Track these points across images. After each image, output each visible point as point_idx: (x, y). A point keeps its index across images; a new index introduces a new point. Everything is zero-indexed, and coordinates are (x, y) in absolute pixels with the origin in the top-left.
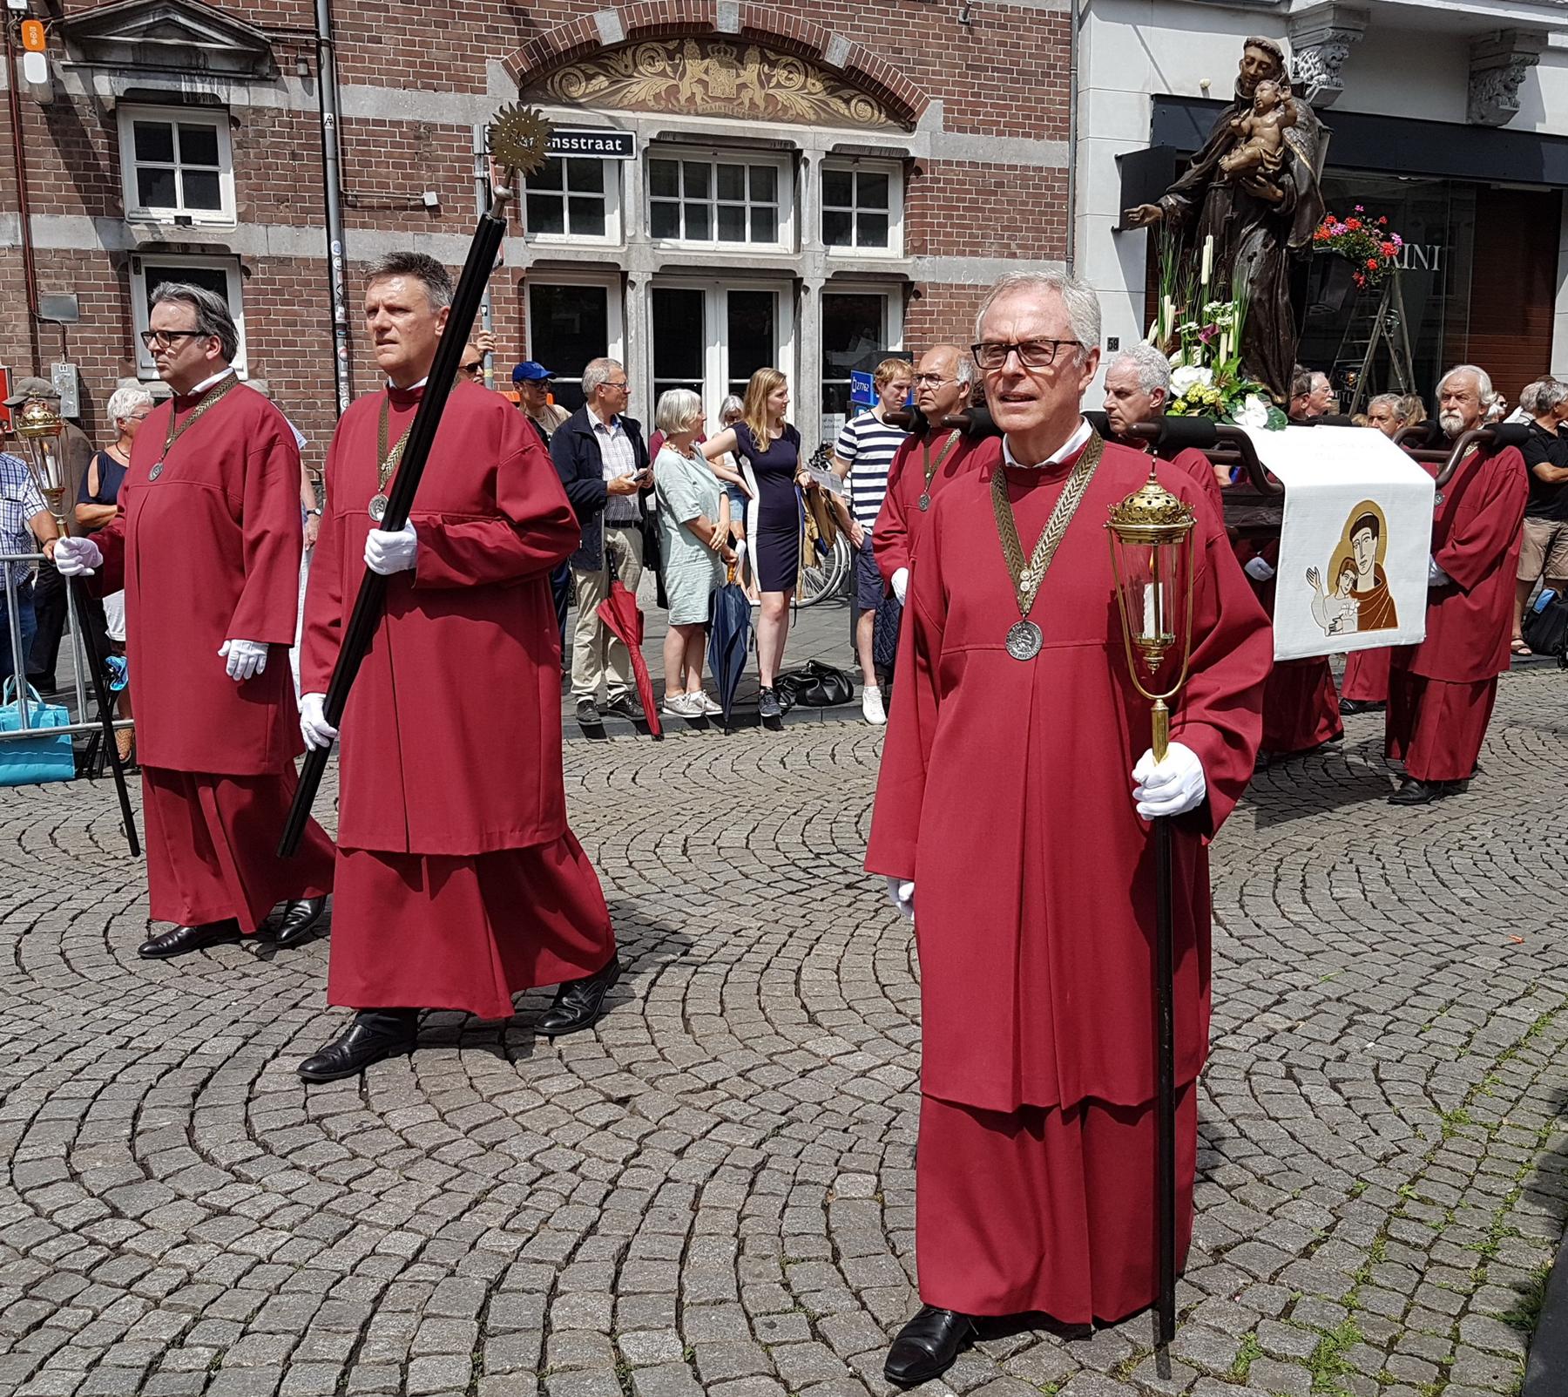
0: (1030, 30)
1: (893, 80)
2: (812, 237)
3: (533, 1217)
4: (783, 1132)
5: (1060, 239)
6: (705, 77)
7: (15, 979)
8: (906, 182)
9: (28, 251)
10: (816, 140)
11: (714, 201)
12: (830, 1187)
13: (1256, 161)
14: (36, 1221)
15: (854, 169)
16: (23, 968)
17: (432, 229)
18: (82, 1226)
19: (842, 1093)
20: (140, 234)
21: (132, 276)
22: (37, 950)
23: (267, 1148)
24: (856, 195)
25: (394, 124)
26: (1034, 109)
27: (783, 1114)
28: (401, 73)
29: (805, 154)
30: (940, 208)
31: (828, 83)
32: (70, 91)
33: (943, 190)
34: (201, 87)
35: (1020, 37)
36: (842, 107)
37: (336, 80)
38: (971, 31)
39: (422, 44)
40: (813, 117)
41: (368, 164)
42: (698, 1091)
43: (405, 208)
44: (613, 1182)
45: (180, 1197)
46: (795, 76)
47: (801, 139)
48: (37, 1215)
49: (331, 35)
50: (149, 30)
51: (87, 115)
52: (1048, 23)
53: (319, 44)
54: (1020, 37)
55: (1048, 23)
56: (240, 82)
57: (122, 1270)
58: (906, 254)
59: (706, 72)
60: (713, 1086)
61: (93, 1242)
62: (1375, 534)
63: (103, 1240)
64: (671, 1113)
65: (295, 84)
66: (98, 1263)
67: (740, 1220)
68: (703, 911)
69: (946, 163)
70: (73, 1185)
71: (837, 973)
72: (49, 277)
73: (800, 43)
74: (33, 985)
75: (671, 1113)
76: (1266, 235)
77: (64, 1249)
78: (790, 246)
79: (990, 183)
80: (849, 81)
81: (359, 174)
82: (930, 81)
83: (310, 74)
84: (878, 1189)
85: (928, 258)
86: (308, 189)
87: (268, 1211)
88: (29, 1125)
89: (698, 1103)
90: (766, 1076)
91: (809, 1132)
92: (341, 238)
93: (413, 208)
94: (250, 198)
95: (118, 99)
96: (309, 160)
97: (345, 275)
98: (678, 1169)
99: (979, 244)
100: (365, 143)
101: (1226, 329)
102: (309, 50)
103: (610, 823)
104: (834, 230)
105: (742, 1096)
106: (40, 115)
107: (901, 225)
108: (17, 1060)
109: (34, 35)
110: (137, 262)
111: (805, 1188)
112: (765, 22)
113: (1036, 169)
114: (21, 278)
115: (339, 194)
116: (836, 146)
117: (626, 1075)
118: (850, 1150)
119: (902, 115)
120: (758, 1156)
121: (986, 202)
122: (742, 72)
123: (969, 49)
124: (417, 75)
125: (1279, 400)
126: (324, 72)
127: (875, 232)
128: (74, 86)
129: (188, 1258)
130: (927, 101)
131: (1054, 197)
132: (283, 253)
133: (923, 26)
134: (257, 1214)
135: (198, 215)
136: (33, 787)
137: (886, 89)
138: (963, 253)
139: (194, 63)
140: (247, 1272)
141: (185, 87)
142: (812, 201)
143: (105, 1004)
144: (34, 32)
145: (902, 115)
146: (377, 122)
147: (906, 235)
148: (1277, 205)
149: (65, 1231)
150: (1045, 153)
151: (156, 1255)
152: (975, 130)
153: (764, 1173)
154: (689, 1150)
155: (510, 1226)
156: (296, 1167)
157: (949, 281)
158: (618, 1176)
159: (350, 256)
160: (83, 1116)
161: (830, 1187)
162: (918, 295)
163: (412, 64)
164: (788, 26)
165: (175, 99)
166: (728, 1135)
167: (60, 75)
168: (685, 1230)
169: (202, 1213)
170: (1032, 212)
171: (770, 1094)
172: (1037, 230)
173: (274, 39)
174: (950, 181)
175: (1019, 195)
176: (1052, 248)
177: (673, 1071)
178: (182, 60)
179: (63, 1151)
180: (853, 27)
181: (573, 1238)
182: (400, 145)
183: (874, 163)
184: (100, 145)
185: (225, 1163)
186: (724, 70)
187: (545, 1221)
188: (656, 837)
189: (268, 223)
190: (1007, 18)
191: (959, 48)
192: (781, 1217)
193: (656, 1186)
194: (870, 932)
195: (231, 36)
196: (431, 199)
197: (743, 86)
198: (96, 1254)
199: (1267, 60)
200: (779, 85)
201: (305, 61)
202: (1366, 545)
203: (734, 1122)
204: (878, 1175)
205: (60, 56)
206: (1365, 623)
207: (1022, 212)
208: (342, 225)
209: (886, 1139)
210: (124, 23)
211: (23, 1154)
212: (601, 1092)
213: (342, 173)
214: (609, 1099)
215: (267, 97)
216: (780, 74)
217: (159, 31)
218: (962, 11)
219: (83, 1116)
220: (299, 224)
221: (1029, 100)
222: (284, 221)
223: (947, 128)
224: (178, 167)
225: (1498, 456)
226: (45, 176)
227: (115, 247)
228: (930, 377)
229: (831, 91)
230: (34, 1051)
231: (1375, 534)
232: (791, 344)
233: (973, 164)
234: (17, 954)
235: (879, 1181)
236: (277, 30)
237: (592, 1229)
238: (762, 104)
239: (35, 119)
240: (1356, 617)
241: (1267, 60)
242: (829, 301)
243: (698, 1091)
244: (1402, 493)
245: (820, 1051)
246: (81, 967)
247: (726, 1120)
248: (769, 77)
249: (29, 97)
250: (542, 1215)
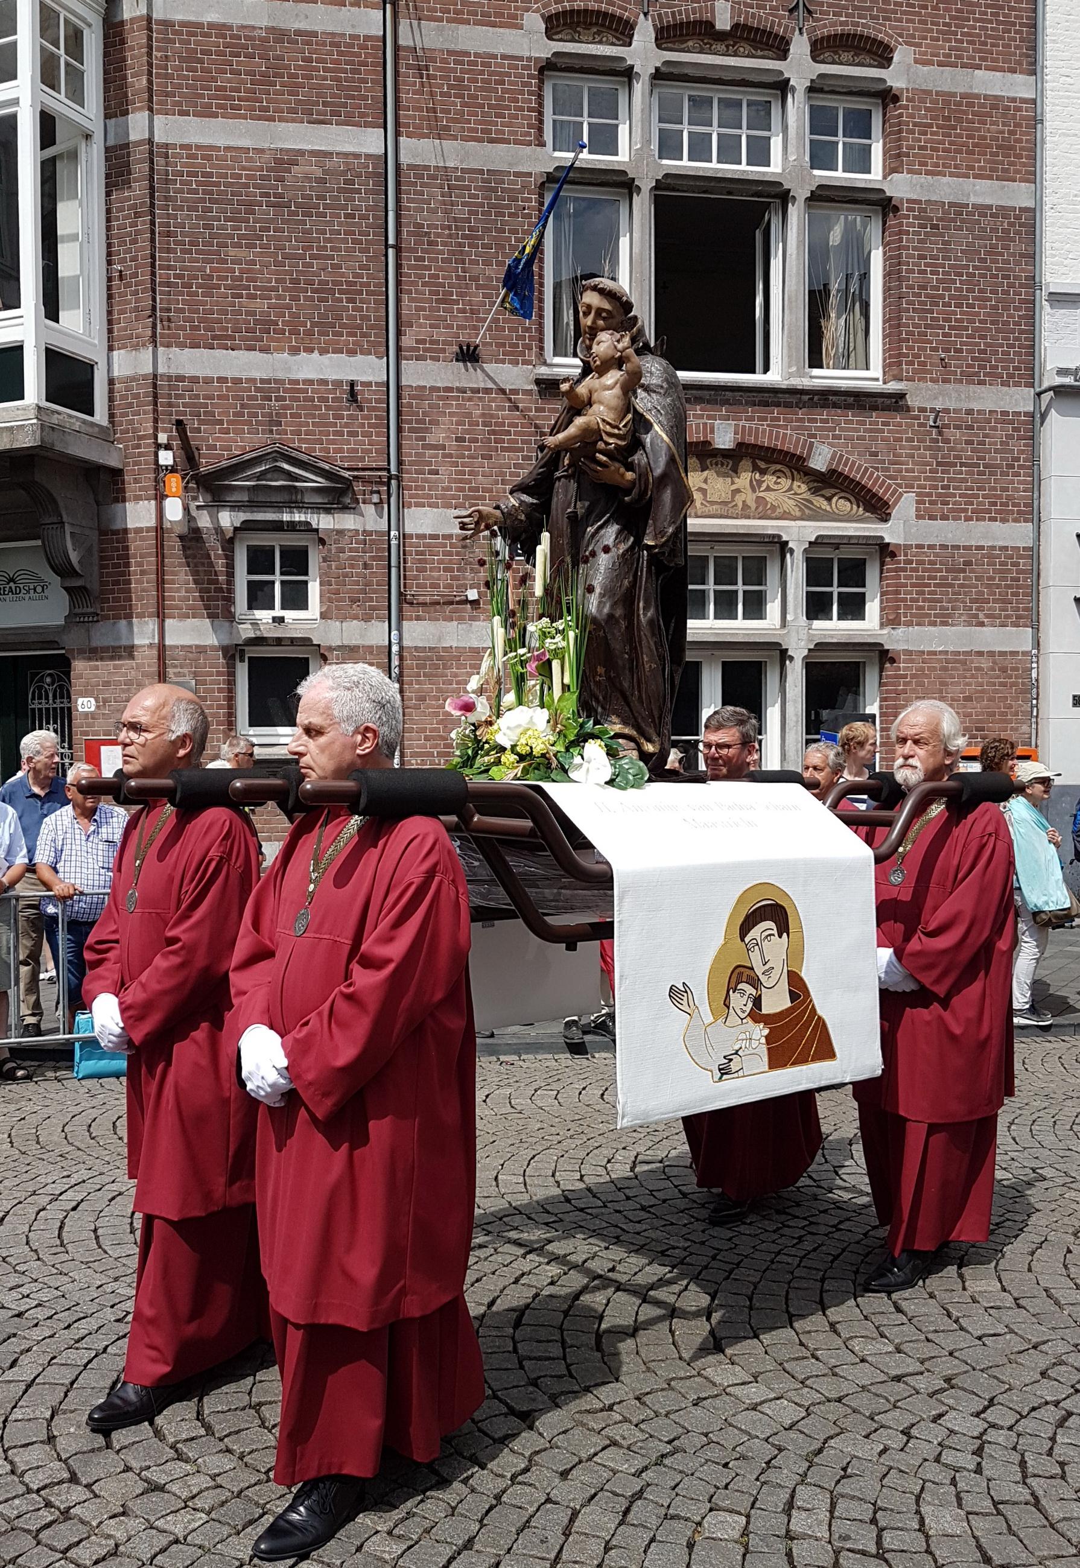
0: (995, 429)
1: (869, 479)
2: (796, 614)
3: (418, 1525)
4: (666, 1461)
5: (1025, 609)
6: (704, 486)
7: (54, 1250)
8: (882, 564)
9: (162, 648)
10: (798, 533)
11: (711, 587)
12: (699, 1524)
13: (591, 436)
14: (9, 1478)
15: (835, 555)
16: (62, 1242)
17: (473, 619)
18: (44, 1487)
19: (731, 1425)
20: (246, 632)
21: (239, 665)
22: (78, 1227)
23: (209, 1429)
24: (836, 576)
25: (445, 537)
26: (1000, 497)
27: (670, 1442)
28: (454, 497)
29: (790, 545)
30: (913, 585)
31: (812, 485)
32: (201, 524)
33: (916, 570)
34: (298, 517)
35: (986, 436)
36: (824, 504)
37: (401, 505)
38: (940, 433)
39: (471, 473)
40: (798, 514)
41: (424, 570)
42: (596, 1412)
43: (452, 603)
44: (498, 1497)
45: (128, 1469)
46: (782, 480)
47: (787, 533)
48: (13, 1472)
49: (399, 470)
50: (261, 476)
51: (213, 544)
52: (1012, 422)
53: (390, 478)
54: (986, 436)
55: (1012, 422)
56: (328, 511)
57: (65, 1534)
58: (882, 625)
59: (705, 481)
60: (610, 1408)
61: (48, 1504)
62: (783, 928)
63: (57, 1503)
64: (564, 1432)
65: (369, 510)
66: (48, 1525)
67: (607, 1549)
68: (638, 1227)
69: (918, 546)
70: (47, 1448)
71: (751, 1299)
72: (176, 667)
73: (787, 453)
74: (66, 1257)
75: (564, 1432)
76: (619, 533)
77: (24, 1508)
78: (777, 622)
79: (958, 562)
80: (830, 482)
81: (416, 578)
82: (903, 478)
83: (381, 502)
84: (745, 1533)
85: (902, 629)
86: (375, 592)
87: (195, 1492)
88: (29, 1386)
89: (592, 1424)
90: (661, 1402)
91: (691, 1464)
92: (400, 629)
93: (458, 603)
94: (330, 600)
95: (236, 529)
96: (378, 569)
97: (401, 658)
98: (565, 1492)
99: (949, 616)
100: (422, 553)
101: (559, 653)
102: (381, 483)
103: (571, 1137)
104: (817, 607)
105: (635, 1421)
106: (178, 544)
107: (877, 601)
108: (36, 1325)
109: (174, 485)
110: (242, 652)
111: (675, 1523)
112: (756, 437)
113: (1001, 548)
114: (155, 669)
115: (400, 594)
116: (818, 537)
117: (531, 1389)
118: (726, 1487)
119: (878, 507)
120: (636, 1485)
121: (955, 579)
122: (736, 480)
123: (939, 449)
124: (466, 498)
125: (650, 748)
126: (393, 500)
127: (853, 607)
128: (204, 521)
129: (117, 1530)
130: (901, 495)
131: (1019, 572)
132: (354, 642)
133: (898, 432)
134: (185, 1495)
135: (290, 615)
136: (113, 1080)
137: (864, 487)
138: (934, 624)
139: (293, 499)
140: (163, 1551)
141: (286, 517)
142: (797, 584)
143: (116, 1279)
144: (174, 482)
145: (878, 507)
146: (434, 537)
147: (882, 609)
148: (628, 492)
149: (29, 1491)
150: (1012, 534)
151: (94, 1524)
152: (945, 518)
153: (639, 1502)
154: (574, 1472)
155: (396, 1532)
156: (229, 1451)
157: (922, 648)
158: (504, 1492)
159: (405, 643)
160: (72, 1383)
161: (699, 1524)
162: (893, 661)
163: (462, 490)
164: (777, 439)
165: (278, 527)
166: (613, 1459)
167: (194, 513)
168: (552, 1556)
169: (141, 1486)
170: (998, 586)
171: (661, 1421)
172: (1004, 601)
173: (355, 477)
174: (922, 562)
175: (986, 571)
176: (1019, 617)
177: (576, 1388)
178: (286, 497)
179: (48, 1414)
180: (835, 437)
181: (448, 1552)
182: (450, 554)
183: (854, 549)
184: (220, 564)
185: (172, 1440)
186: (721, 479)
187: (427, 1531)
188: (607, 1152)
189: (343, 619)
190: (974, 420)
191: (929, 448)
192: (645, 1552)
193: (536, 1505)
194: (790, 1260)
195: (322, 476)
196: (473, 594)
197: (738, 491)
198: (47, 1516)
199: (606, 306)
200: (768, 489)
201: (378, 492)
202: (769, 949)
203: (621, 1447)
204: (748, 1516)
205: (195, 499)
206: (778, 1058)
207: (988, 586)
208: (401, 618)
209: (762, 1478)
210: (243, 470)
211: (18, 1414)
212: (507, 1404)
213: (403, 577)
214: (512, 1412)
215: (348, 522)
216: (770, 480)
217: (269, 476)
218: (932, 417)
219: (72, 1383)
220: (367, 619)
221: (995, 489)
222: (356, 618)
223: (919, 517)
224: (277, 578)
225: (971, 817)
226: (178, 590)
227: (226, 642)
228: (135, 727)
229: (815, 491)
230: (50, 1318)
231: (783, 928)
232: (778, 706)
233: (944, 547)
234: (61, 1228)
235: (748, 1523)
236: (357, 469)
237: (469, 1544)
238: (753, 506)
239: (173, 546)
240: (764, 1049)
241: (606, 306)
242: (811, 667)
243: (596, 1412)
244: (831, 871)
245: (717, 1380)
246: (106, 1243)
247: (614, 1443)
248: (760, 483)
249: (170, 531)
250: (427, 1524)
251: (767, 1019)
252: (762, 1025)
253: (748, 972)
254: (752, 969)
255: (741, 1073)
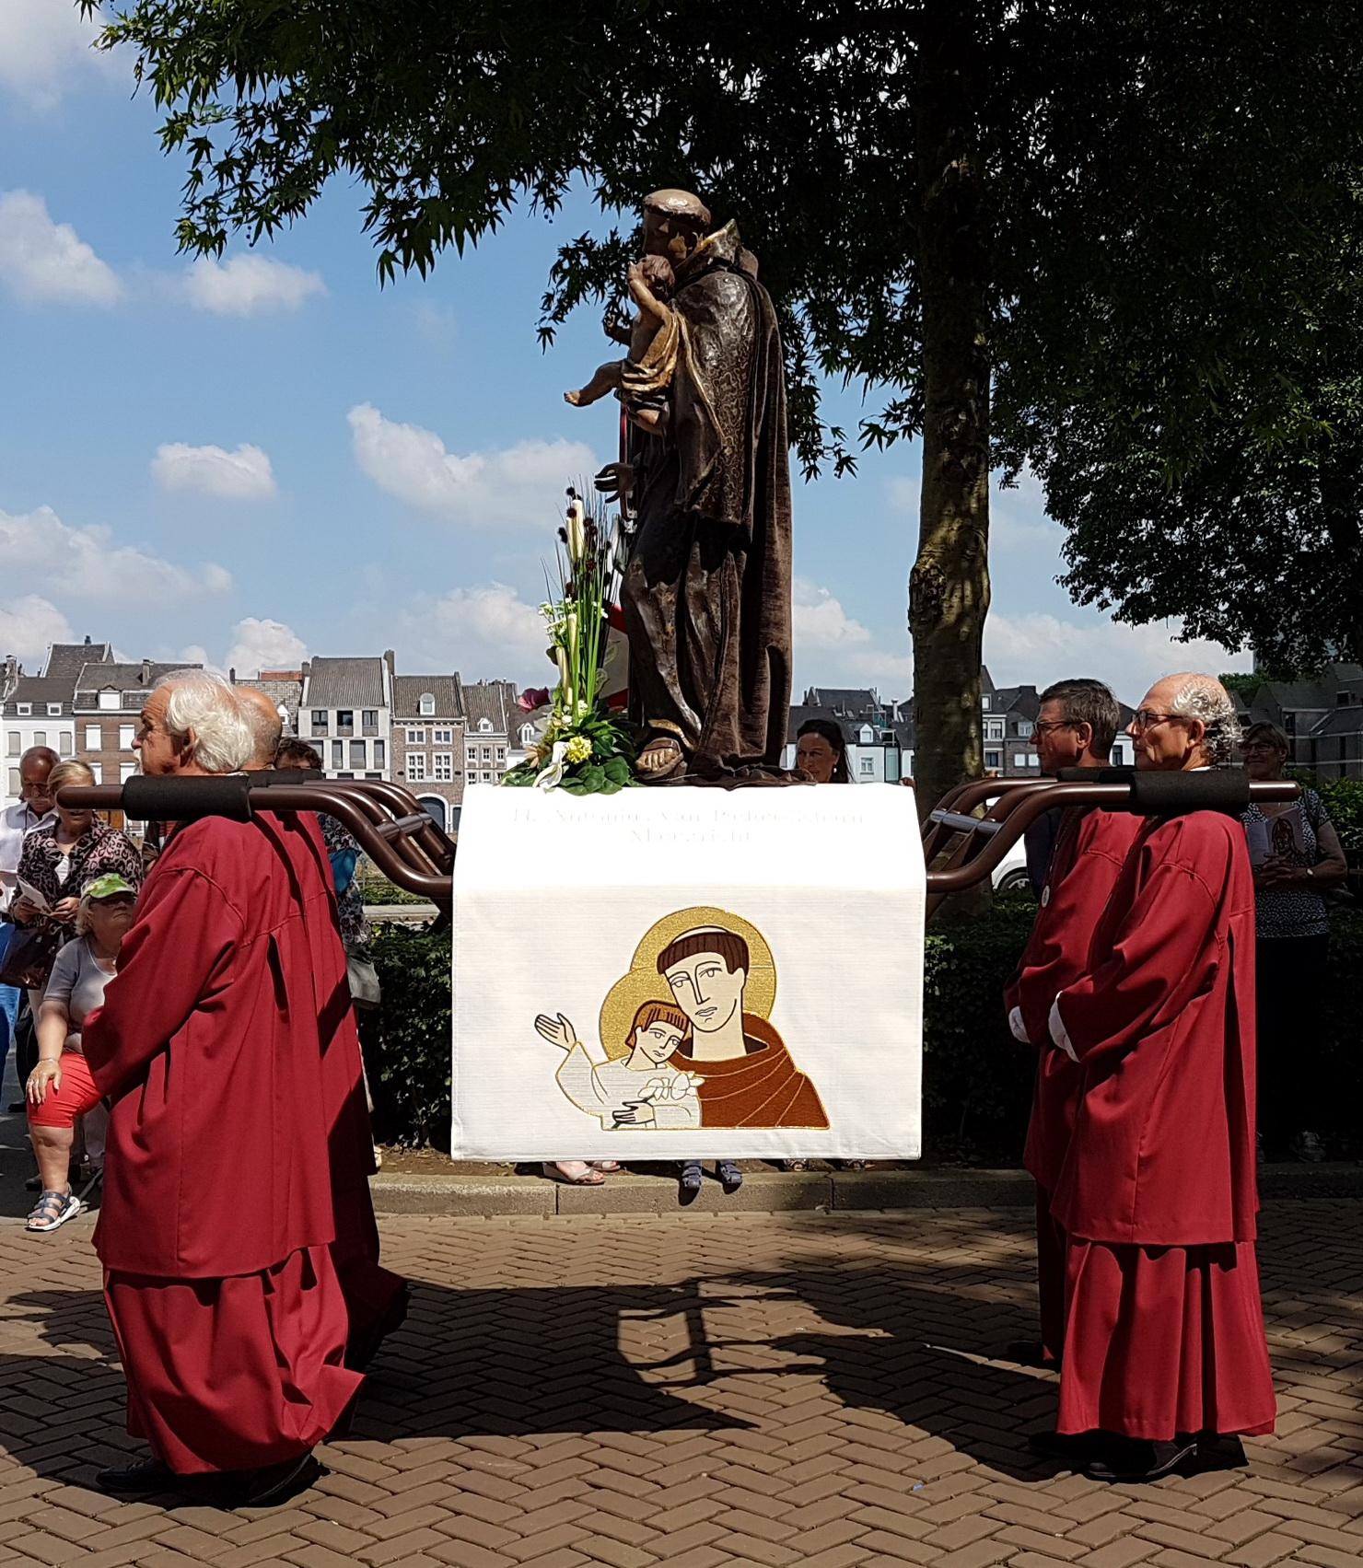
202: (711, 989)
251: (700, 1068)
252: (691, 1074)
253: (672, 1010)
254: (678, 1006)
255: (651, 1125)
